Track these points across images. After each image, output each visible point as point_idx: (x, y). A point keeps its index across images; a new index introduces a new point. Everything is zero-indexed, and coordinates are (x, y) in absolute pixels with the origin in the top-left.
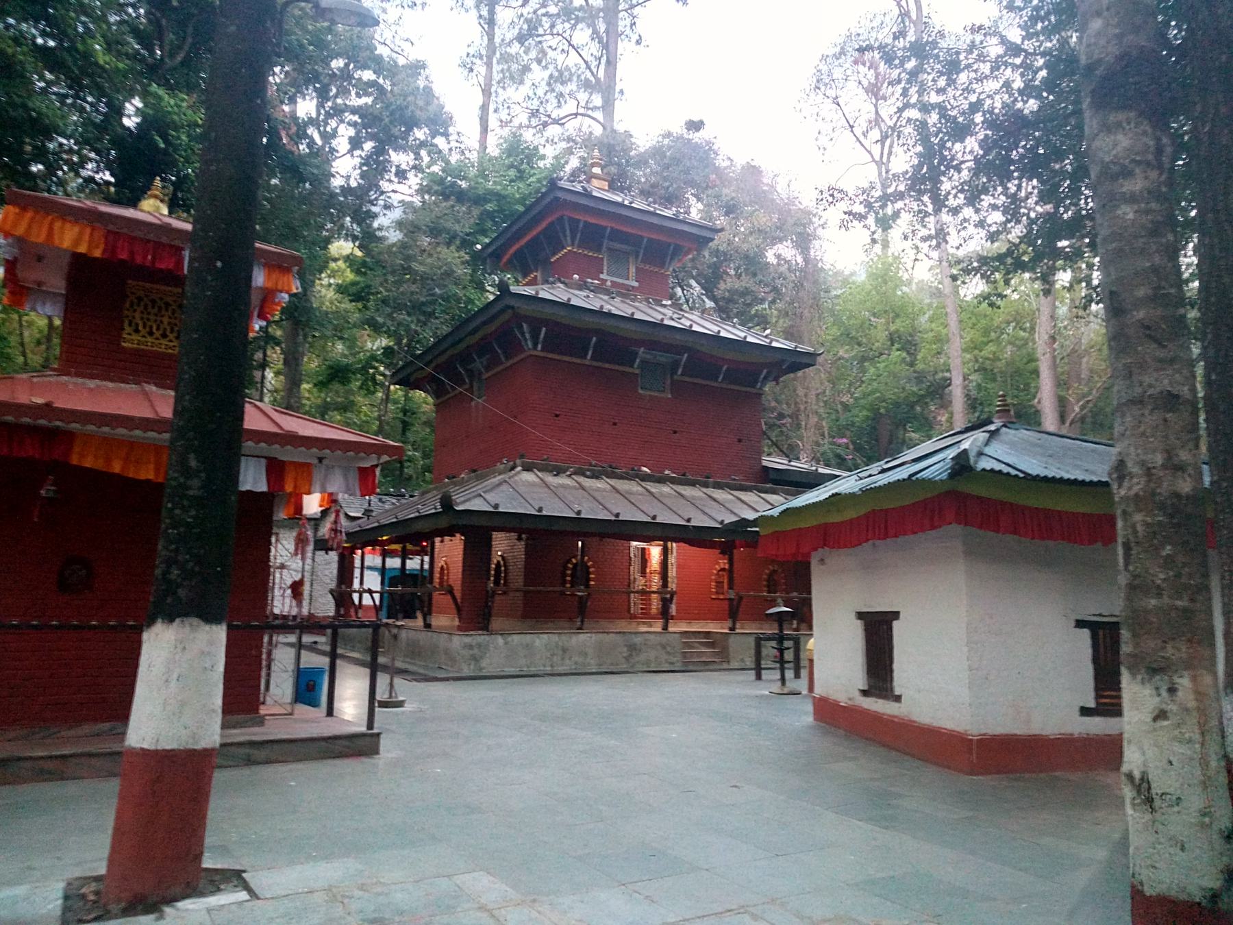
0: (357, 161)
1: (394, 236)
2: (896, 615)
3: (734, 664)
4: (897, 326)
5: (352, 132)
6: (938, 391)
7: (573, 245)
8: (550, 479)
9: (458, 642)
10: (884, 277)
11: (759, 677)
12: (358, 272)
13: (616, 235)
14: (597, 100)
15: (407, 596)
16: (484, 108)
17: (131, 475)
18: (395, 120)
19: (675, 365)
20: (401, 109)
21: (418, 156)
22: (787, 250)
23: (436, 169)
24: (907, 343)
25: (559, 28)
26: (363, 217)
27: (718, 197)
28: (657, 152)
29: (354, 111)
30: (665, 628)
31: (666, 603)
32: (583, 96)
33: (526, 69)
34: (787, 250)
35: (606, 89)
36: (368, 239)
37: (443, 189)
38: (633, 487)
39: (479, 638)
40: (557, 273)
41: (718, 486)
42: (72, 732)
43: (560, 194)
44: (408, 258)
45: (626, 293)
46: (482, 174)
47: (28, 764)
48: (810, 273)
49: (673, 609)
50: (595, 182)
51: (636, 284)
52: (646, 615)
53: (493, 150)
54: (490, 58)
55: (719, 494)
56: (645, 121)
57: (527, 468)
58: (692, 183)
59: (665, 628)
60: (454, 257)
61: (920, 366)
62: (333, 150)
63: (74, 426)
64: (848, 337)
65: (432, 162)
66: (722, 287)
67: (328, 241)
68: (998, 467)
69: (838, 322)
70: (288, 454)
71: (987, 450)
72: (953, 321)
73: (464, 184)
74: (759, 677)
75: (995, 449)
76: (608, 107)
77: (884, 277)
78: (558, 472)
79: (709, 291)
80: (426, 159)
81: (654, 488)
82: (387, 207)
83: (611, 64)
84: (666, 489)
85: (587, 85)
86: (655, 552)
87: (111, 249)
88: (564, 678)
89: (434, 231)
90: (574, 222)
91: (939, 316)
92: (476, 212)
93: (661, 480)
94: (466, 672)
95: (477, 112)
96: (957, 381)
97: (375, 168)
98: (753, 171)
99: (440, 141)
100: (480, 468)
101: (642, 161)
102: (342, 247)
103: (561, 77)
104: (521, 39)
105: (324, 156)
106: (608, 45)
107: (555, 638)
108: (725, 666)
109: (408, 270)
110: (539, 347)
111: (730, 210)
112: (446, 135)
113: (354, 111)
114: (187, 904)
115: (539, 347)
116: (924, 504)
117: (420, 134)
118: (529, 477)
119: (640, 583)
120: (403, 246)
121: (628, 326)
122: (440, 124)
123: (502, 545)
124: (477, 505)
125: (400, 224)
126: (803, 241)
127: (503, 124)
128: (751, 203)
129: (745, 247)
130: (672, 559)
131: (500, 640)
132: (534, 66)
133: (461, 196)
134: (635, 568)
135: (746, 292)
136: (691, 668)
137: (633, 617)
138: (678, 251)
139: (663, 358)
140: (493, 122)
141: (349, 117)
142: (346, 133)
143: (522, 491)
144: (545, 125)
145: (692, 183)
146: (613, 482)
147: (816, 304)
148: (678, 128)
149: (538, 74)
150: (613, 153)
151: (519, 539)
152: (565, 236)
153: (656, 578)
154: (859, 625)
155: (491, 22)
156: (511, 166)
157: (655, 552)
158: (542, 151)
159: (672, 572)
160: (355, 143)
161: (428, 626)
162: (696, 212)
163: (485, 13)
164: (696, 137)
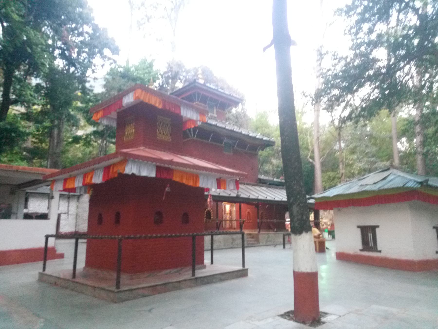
2: (378, 226)
3: (261, 244)
7: (198, 101)
11: (284, 247)
13: (211, 99)
18: (97, 44)
19: (235, 144)
42: (160, 274)
43: (196, 84)
47: (171, 285)
51: (216, 116)
63: (173, 167)
70: (223, 176)
74: (284, 247)
87: (164, 106)
88: (224, 250)
90: (199, 94)
108: (258, 244)
110: (195, 136)
115: (195, 136)
116: (399, 194)
121: (224, 131)
136: (249, 245)
138: (229, 105)
139: (230, 142)
152: (195, 99)
153: (228, 216)
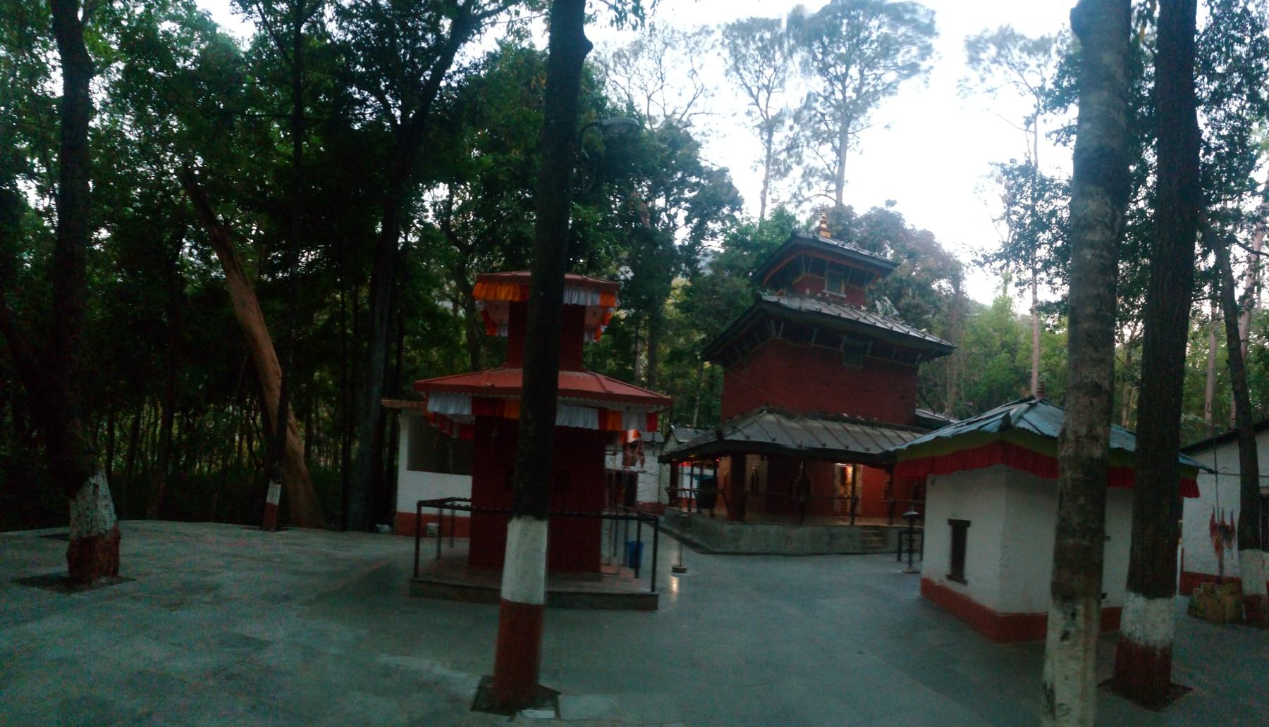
0: (689, 230)
1: (708, 272)
4: (1007, 338)
5: (686, 213)
6: (1026, 379)
8: (784, 421)
9: (727, 528)
10: (1003, 306)
12: (688, 295)
14: (833, 187)
15: (708, 494)
16: (764, 192)
17: (581, 425)
20: (714, 195)
21: (724, 224)
22: (945, 284)
23: (734, 230)
24: (1012, 349)
25: (812, 144)
26: (692, 263)
27: (903, 247)
28: (867, 218)
29: (686, 200)
30: (852, 523)
31: (854, 505)
32: (824, 184)
33: (788, 169)
34: (945, 284)
35: (838, 180)
36: (694, 275)
37: (735, 242)
38: (837, 426)
39: (739, 526)
40: (796, 291)
41: (888, 427)
44: (715, 285)
45: (838, 302)
46: (761, 231)
48: (959, 302)
49: (859, 509)
50: (823, 233)
52: (843, 513)
53: (767, 218)
54: (768, 162)
55: (888, 432)
56: (861, 200)
57: (770, 412)
58: (889, 238)
59: (852, 523)
60: (740, 283)
61: (1017, 364)
62: (675, 225)
64: (979, 341)
65: (732, 226)
66: (904, 301)
67: (671, 279)
68: (1027, 426)
69: (974, 332)
70: (611, 406)
71: (1027, 416)
72: (1036, 340)
73: (749, 238)
75: (1031, 416)
76: (839, 190)
77: (1003, 306)
78: (790, 417)
79: (895, 303)
80: (729, 225)
81: (850, 427)
82: (705, 255)
83: (842, 164)
84: (857, 429)
85: (826, 177)
86: (850, 470)
89: (731, 267)
91: (1030, 336)
92: (755, 255)
93: (855, 422)
94: (731, 549)
95: (759, 195)
96: (1035, 375)
97: (699, 233)
98: (928, 236)
99: (737, 214)
100: (745, 413)
101: (858, 223)
102: (679, 281)
103: (809, 173)
104: (788, 149)
105: (670, 230)
106: (840, 152)
107: (781, 529)
109: (715, 292)
111: (912, 255)
112: (740, 210)
113: (686, 200)
114: (529, 713)
117: (726, 210)
118: (770, 418)
119: (841, 491)
120: (712, 277)
122: (736, 203)
123: (754, 463)
124: (738, 437)
125: (711, 265)
126: (956, 280)
127: (774, 201)
128: (925, 253)
129: (918, 279)
130: (859, 475)
131: (749, 528)
132: (794, 166)
133: (746, 246)
134: (837, 482)
135: (917, 306)
137: (835, 515)
140: (768, 201)
141: (684, 204)
142: (682, 215)
143: (767, 427)
144: (800, 202)
145: (889, 238)
146: (825, 423)
147: (961, 318)
148: (881, 205)
149: (797, 171)
150: (839, 217)
151: (762, 459)
153: (850, 488)
154: (967, 577)
155: (769, 141)
156: (777, 226)
157: (850, 470)
158: (797, 218)
159: (859, 484)
160: (688, 220)
161: (712, 515)
162: (890, 254)
163: (766, 137)
164: (892, 210)
